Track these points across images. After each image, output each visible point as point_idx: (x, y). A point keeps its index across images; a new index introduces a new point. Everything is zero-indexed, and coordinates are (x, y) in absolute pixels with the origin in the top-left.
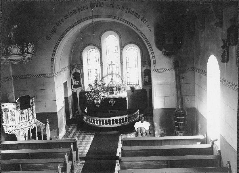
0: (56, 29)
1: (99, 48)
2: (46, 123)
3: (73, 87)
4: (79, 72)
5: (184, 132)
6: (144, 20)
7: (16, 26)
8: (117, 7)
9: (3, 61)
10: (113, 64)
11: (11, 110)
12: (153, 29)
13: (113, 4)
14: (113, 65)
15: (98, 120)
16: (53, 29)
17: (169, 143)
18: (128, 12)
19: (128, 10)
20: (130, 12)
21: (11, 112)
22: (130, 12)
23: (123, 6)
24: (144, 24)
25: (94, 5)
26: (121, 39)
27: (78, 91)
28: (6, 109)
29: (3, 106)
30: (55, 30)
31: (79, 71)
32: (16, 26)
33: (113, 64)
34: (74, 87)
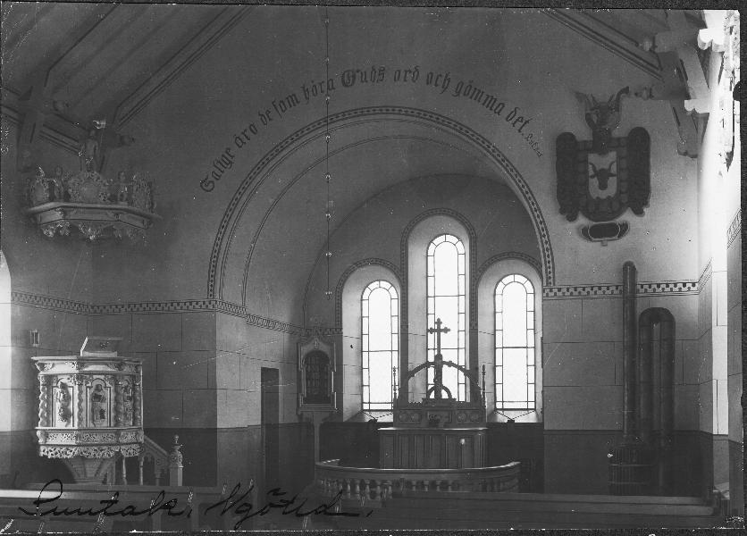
0: (232, 157)
1: (401, 277)
2: (171, 451)
3: (301, 399)
4: (328, 352)
5: (622, 431)
6: (516, 117)
7: (104, 123)
8: (427, 80)
9: (56, 224)
10: (442, 327)
11: (65, 380)
12: (677, 321)
13: (417, 70)
14: (439, 327)
15: (358, 482)
16: (223, 156)
17: (425, 248)
18: (464, 95)
19: (463, 90)
20: (470, 94)
21: (64, 386)
22: (470, 94)
23: (447, 75)
24: (505, 121)
25: (354, 77)
26: (475, 242)
27: (317, 415)
28: (50, 379)
29: (42, 366)
30: (230, 158)
31: (324, 348)
32: (104, 123)
33: (442, 327)
34: (306, 400)
